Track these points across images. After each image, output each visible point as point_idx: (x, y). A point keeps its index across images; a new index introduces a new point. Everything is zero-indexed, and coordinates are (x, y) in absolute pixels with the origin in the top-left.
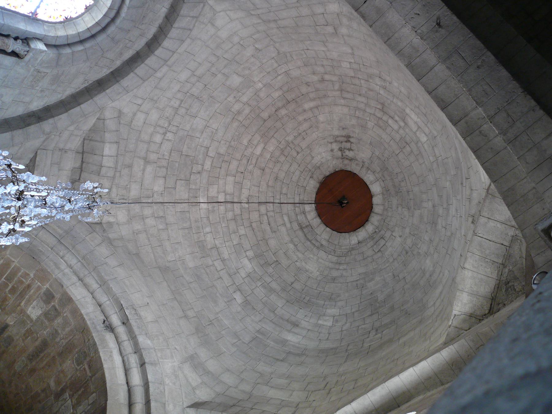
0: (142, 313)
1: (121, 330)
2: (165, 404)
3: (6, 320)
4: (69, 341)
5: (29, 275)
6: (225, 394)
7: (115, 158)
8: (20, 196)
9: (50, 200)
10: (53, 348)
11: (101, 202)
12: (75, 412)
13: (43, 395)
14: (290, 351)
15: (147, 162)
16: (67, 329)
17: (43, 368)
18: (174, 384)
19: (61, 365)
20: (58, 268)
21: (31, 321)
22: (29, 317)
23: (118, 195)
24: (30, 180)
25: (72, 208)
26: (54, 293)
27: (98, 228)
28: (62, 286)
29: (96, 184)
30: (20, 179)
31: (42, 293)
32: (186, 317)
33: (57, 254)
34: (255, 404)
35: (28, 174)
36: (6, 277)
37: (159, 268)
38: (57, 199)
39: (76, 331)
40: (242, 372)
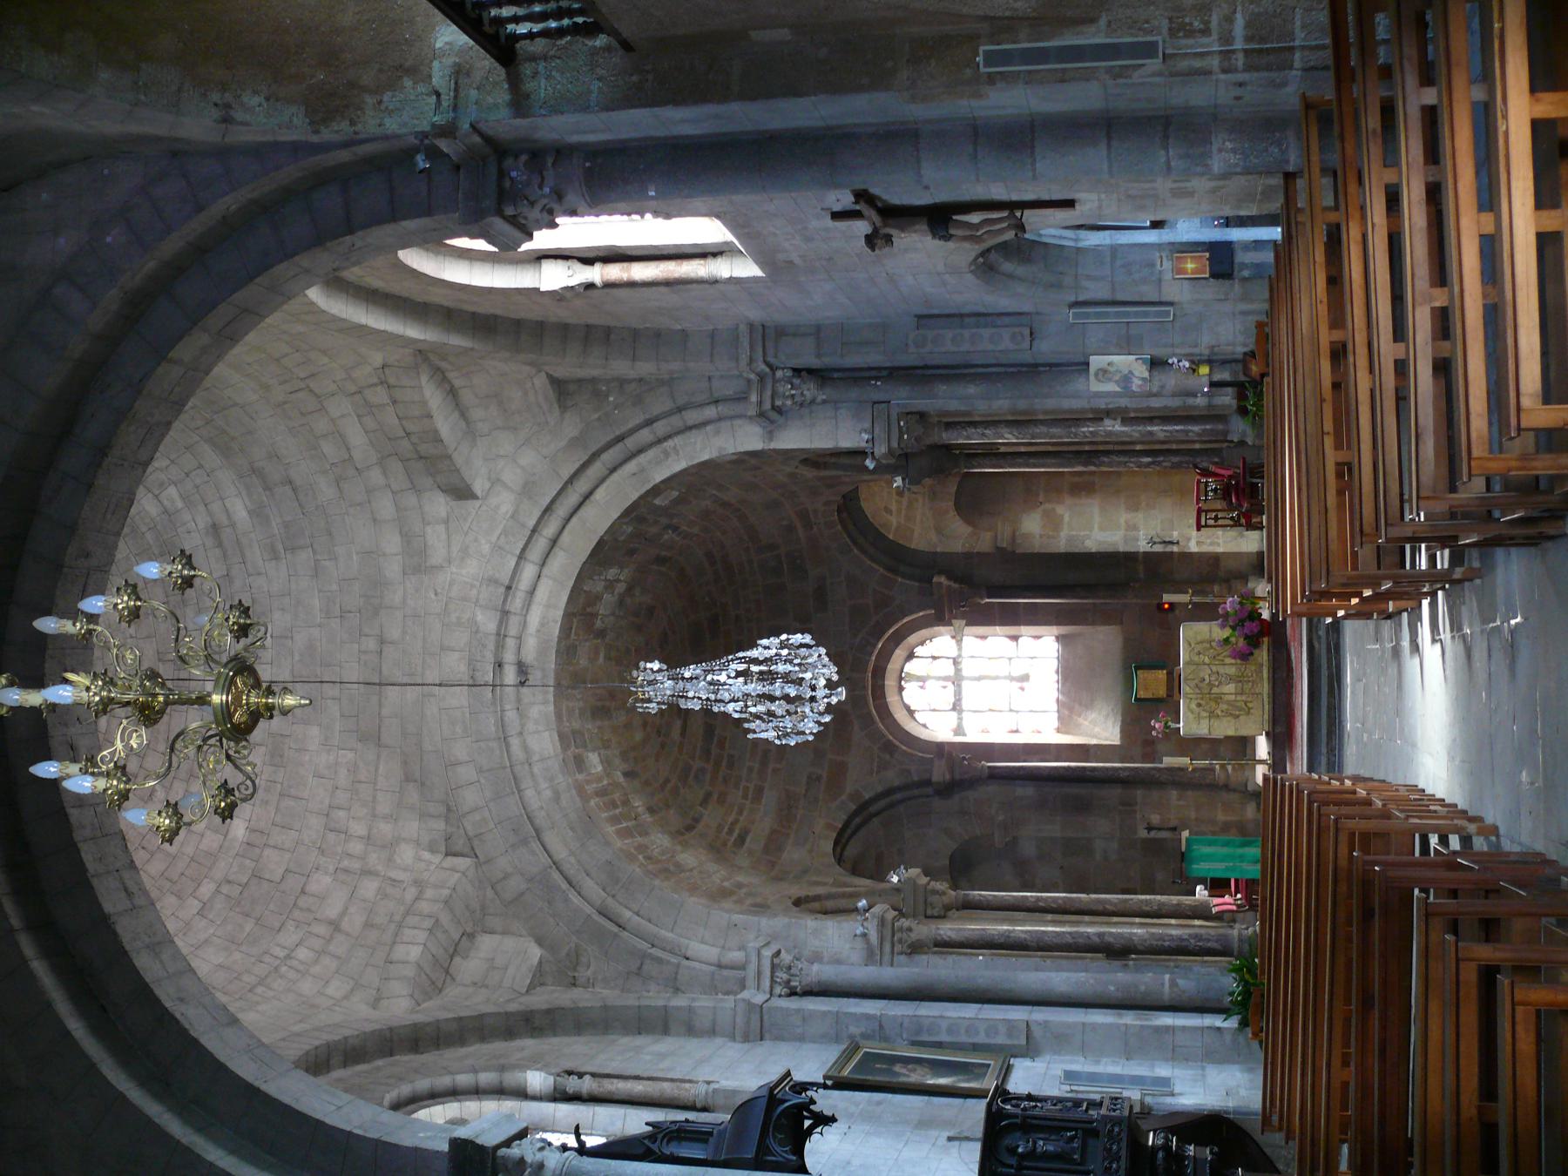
0: (463, 668)
6: (411, 486)
14: (264, 490)
15: (335, 926)
18: (476, 540)
21: (599, 754)
27: (460, 845)
32: (382, 641)
40: (359, 504)
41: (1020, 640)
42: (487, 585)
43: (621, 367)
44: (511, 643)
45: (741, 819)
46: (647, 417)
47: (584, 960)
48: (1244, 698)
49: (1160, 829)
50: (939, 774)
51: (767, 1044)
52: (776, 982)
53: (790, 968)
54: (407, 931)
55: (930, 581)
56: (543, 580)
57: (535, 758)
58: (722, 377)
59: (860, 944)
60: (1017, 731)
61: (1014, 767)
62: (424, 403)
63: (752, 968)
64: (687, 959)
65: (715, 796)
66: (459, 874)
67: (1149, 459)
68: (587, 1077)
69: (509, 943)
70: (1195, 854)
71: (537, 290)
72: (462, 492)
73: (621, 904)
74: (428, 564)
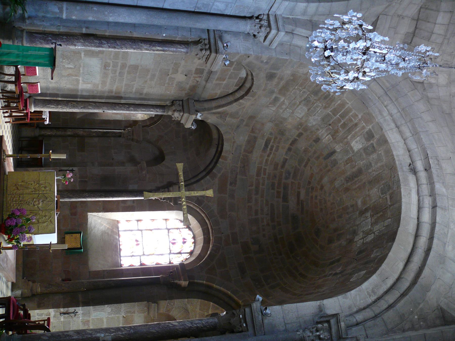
0: (444, 165)
1: (423, 175)
2: (445, 244)
3: (335, 147)
4: (379, 173)
5: (357, 116)
7: (447, 26)
8: (365, 51)
9: (389, 57)
10: (365, 176)
11: (431, 64)
12: (372, 228)
13: (351, 209)
16: (379, 164)
17: (355, 189)
19: (369, 191)
20: (381, 114)
21: (353, 151)
22: (352, 148)
23: (443, 60)
24: (376, 39)
25: (406, 66)
26: (374, 134)
27: (419, 86)
28: (382, 129)
29: (429, 48)
30: (368, 37)
31: (365, 132)
33: (382, 103)
35: (374, 34)
36: (340, 114)
38: (394, 57)
39: (386, 167)
45: (266, 158)
46: (395, 308)
48: (19, 192)
56: (416, 217)
65: (279, 167)
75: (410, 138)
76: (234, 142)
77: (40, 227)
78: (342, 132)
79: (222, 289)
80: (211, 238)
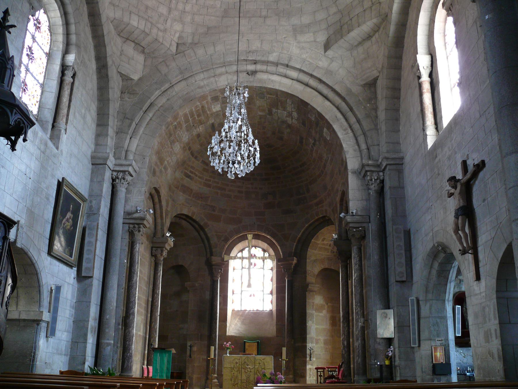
0: (254, 48)
5: (197, 105)
6: (329, 25)
18: (307, 52)
21: (220, 111)
22: (217, 112)
27: (181, 48)
31: (211, 101)
32: (265, 17)
34: (349, 15)
37: (223, 17)
40: (321, 5)
41: (271, 295)
42: (288, 57)
43: (382, 105)
44: (264, 68)
45: (197, 177)
47: (132, 96)
49: (190, 351)
50: (215, 260)
51: (90, 166)
52: (118, 173)
53: (124, 179)
54: (144, 22)
55: (294, 256)
56: (291, 81)
57: (217, 79)
58: (379, 150)
59: (134, 209)
60: (233, 293)
61: (217, 290)
62: (364, 23)
63: (124, 162)
64: (130, 138)
65: (206, 167)
66: (169, 47)
67: (346, 344)
68: (72, 80)
69: (140, 67)
70: (164, 355)
71: (417, 53)
72: (327, 46)
73: (155, 113)
74: (297, 34)
75: (227, 69)
76: (183, 204)
77: (268, 368)
78: (203, 118)
79: (302, 231)
80: (256, 233)
